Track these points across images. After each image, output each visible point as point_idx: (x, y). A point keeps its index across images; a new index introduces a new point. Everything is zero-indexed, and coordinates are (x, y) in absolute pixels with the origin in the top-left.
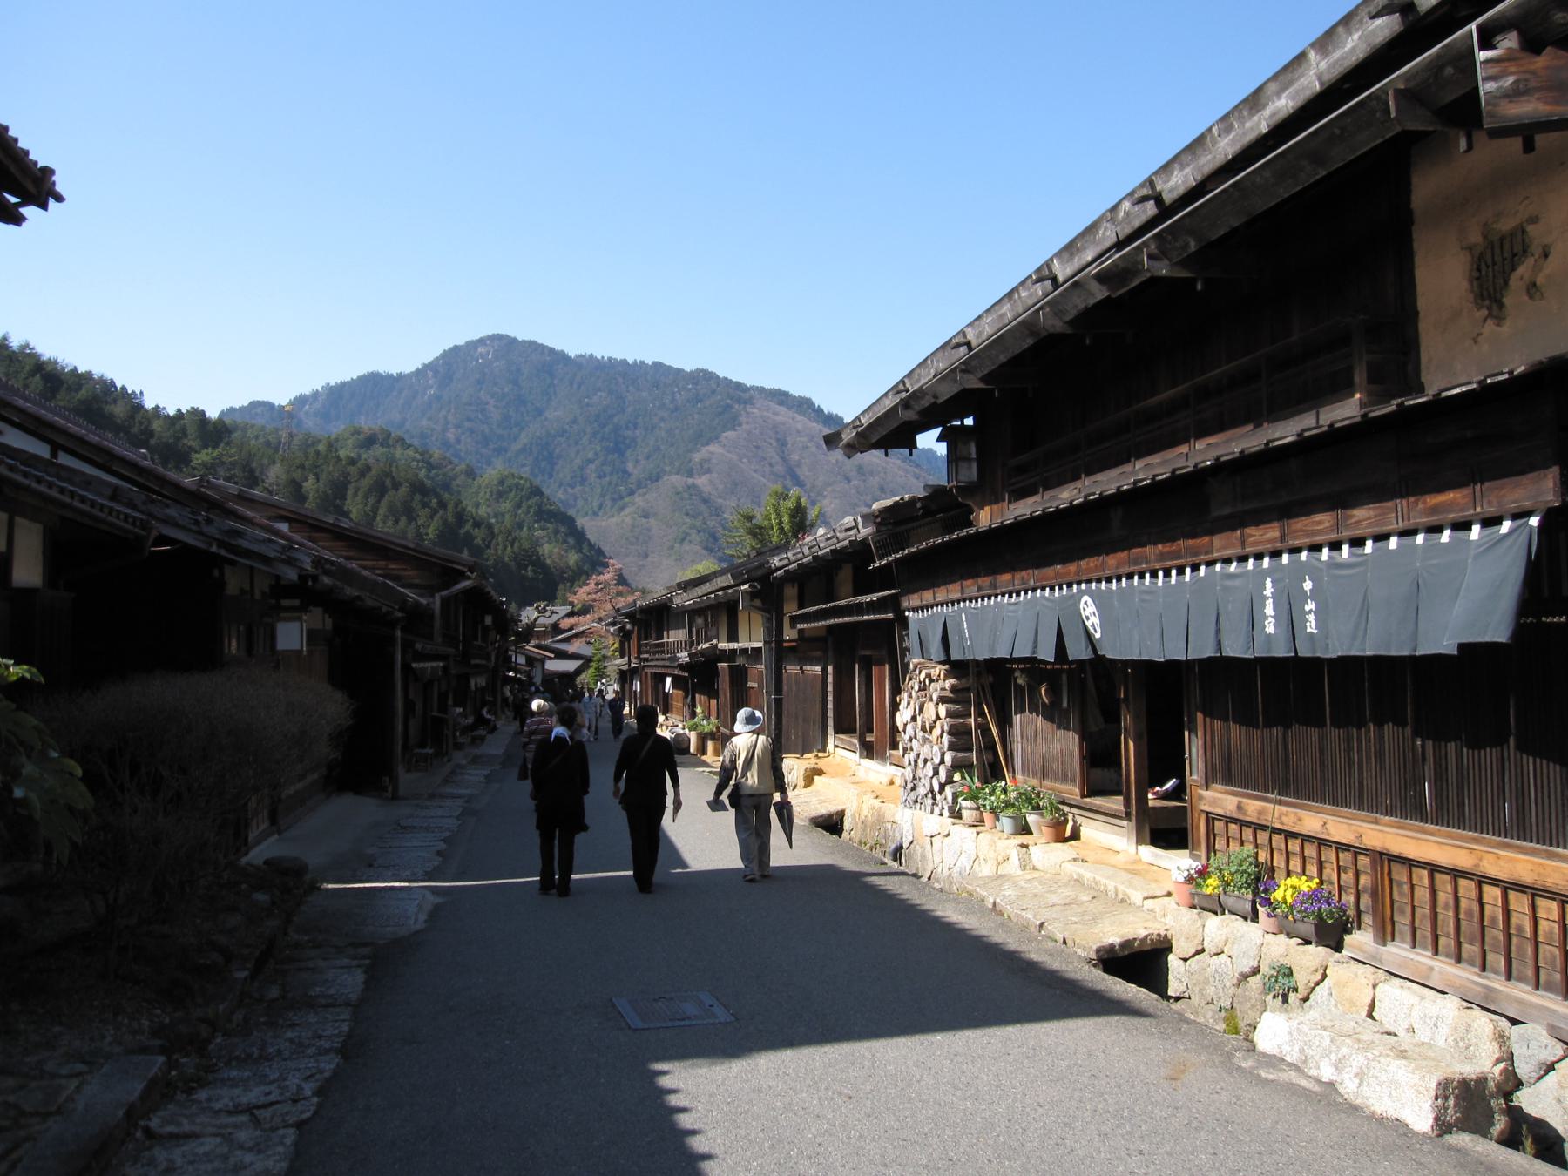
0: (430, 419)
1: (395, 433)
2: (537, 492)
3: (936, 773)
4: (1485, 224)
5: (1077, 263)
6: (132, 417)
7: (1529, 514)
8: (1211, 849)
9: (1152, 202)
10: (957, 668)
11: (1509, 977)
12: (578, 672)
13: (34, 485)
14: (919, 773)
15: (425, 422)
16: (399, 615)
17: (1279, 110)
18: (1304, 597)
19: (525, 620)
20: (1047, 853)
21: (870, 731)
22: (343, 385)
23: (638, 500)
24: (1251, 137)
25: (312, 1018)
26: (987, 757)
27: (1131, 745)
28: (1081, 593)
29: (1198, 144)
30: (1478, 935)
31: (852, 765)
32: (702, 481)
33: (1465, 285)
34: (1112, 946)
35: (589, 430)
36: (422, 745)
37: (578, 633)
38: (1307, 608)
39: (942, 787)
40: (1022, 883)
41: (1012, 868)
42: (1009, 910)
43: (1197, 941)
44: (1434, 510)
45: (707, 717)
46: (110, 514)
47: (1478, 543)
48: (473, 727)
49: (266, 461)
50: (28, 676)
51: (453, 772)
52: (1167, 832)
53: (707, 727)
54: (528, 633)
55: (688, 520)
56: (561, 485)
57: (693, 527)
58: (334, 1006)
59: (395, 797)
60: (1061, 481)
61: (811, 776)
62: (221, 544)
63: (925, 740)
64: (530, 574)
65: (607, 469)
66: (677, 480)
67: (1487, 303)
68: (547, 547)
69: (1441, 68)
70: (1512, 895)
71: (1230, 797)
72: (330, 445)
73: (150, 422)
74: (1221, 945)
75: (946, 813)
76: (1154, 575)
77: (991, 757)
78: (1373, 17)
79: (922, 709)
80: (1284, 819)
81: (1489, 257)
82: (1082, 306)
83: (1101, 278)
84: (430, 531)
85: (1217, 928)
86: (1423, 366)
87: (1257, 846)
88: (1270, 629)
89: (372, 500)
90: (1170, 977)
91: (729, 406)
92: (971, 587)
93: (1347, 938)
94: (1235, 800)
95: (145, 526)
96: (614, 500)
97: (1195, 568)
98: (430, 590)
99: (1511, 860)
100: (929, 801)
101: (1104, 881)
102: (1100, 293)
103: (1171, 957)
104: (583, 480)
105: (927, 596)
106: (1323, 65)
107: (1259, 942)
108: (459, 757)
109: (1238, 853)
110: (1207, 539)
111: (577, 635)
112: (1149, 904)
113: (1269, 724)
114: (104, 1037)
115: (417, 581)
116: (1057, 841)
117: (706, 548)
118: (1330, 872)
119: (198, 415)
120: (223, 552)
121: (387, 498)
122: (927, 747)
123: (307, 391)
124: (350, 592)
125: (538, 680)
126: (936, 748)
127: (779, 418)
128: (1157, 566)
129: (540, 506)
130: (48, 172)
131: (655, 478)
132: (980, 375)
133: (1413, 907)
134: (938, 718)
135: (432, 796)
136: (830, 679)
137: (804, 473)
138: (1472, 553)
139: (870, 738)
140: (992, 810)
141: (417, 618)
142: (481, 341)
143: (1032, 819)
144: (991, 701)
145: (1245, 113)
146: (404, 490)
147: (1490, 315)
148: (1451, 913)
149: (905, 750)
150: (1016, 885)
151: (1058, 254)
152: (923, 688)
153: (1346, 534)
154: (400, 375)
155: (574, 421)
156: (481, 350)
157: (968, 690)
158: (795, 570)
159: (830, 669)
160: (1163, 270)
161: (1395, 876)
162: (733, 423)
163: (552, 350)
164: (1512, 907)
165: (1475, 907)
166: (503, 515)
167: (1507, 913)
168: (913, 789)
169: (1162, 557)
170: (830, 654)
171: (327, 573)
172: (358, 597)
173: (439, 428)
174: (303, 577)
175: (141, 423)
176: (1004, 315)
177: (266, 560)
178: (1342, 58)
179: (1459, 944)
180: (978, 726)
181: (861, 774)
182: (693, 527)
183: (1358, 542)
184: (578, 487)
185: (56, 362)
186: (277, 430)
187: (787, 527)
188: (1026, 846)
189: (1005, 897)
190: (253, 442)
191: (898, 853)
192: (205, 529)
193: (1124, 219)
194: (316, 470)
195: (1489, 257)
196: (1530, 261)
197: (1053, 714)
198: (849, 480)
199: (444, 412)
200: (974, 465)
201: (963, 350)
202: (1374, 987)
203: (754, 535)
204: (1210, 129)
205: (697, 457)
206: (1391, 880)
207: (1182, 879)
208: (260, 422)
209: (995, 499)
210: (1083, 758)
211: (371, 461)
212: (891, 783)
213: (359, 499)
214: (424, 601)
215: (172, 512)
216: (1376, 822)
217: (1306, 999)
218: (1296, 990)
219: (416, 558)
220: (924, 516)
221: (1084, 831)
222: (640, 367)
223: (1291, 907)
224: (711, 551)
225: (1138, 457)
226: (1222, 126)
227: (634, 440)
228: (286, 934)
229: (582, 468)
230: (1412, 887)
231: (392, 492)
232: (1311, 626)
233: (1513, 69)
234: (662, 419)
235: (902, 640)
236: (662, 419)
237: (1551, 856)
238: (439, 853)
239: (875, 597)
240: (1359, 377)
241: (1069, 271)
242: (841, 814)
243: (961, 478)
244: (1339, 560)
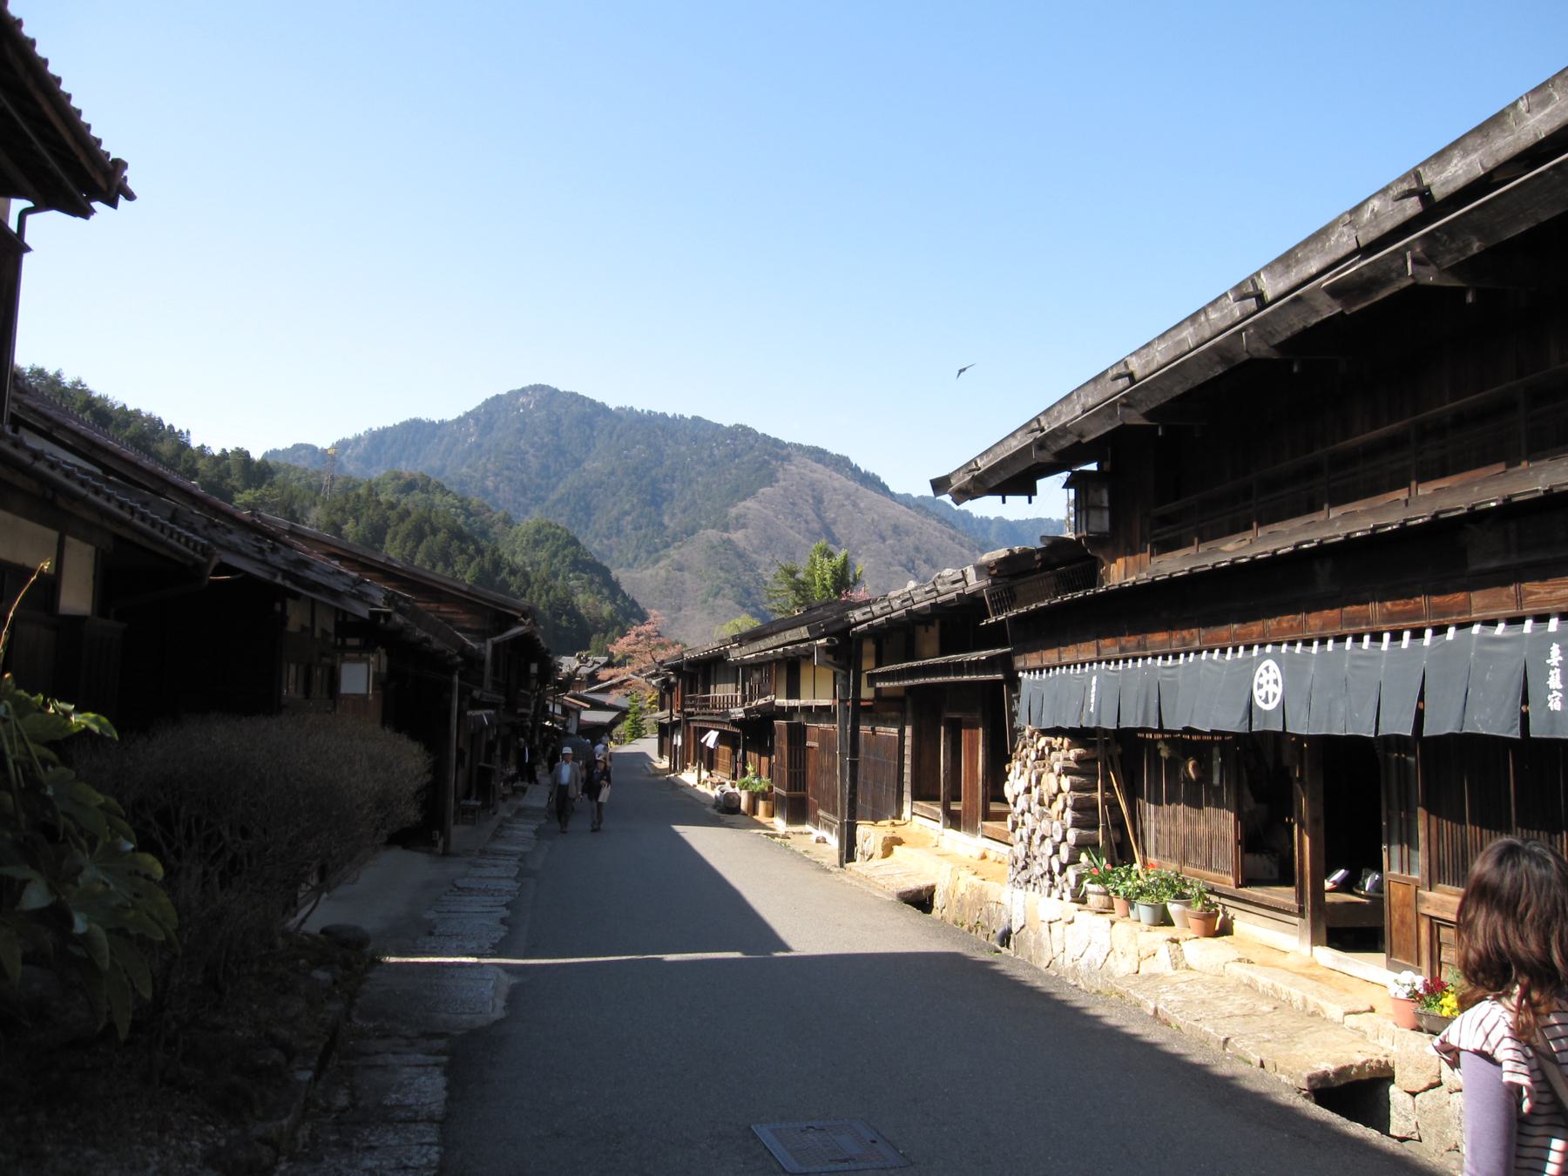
1: (434, 479)
2: (574, 542)
3: (1056, 851)
5: (1294, 277)
6: (178, 456)
9: (1415, 199)
12: (614, 724)
13: (92, 496)
14: (1035, 850)
15: (464, 470)
16: (459, 659)
19: (565, 670)
20: (1205, 953)
22: (385, 430)
25: (392, 1139)
32: (737, 536)
34: (1326, 1074)
37: (617, 685)
39: (1063, 868)
40: (1183, 986)
41: (1162, 964)
42: (1178, 1019)
45: (758, 775)
46: (171, 536)
48: (514, 779)
49: (307, 503)
50: (95, 728)
51: (501, 826)
52: (1354, 932)
54: (570, 681)
55: (722, 574)
56: (597, 536)
57: (727, 581)
58: (415, 1121)
60: (1238, 526)
61: (890, 845)
62: (287, 575)
63: (1043, 815)
64: (564, 624)
65: (643, 521)
66: (712, 534)
68: (581, 596)
72: (370, 489)
73: (195, 461)
75: (1067, 896)
77: (1118, 836)
79: (1040, 783)
83: (1334, 291)
84: (467, 577)
89: (410, 545)
90: (1392, 1113)
91: (768, 462)
95: (206, 552)
96: (649, 552)
98: (482, 635)
100: (1046, 882)
101: (1286, 989)
102: (1329, 309)
103: (1392, 1089)
104: (619, 532)
105: (1050, 656)
110: (1461, 596)
114: (147, 1165)
115: (468, 625)
116: (1208, 935)
117: (739, 603)
119: (243, 456)
120: (288, 584)
121: (425, 543)
122: (1045, 823)
123: (350, 436)
125: (573, 730)
126: (1057, 824)
130: (120, 165)
132: (1144, 409)
134: (1060, 790)
135: (483, 853)
136: (908, 742)
137: (839, 530)
139: (954, 807)
140: (1127, 898)
141: (472, 661)
142: (523, 391)
143: (1174, 909)
144: (1118, 769)
146: (442, 536)
149: (1015, 824)
150: (1174, 986)
151: (1269, 268)
152: (1041, 757)
154: (442, 423)
155: (612, 473)
156: (522, 400)
159: (908, 731)
160: (1430, 278)
162: (770, 479)
163: (592, 402)
166: (539, 564)
168: (1024, 868)
169: (1390, 617)
171: (400, 610)
172: (426, 640)
173: (478, 476)
174: (375, 615)
175: (186, 461)
176: (1184, 340)
177: (334, 594)
180: (1105, 801)
182: (727, 581)
184: (614, 539)
185: (106, 399)
186: (319, 473)
187: (828, 583)
188: (1177, 941)
189: (1167, 1001)
190: (295, 484)
191: (1005, 938)
192: (271, 558)
193: (1370, 221)
194: (356, 514)
198: (884, 539)
200: (1106, 515)
203: (798, 591)
204: (1514, 105)
207: (1404, 996)
208: (302, 464)
209: (1132, 550)
210: (1238, 842)
211: (410, 506)
212: (984, 857)
213: (397, 543)
214: (475, 646)
215: (235, 538)
220: (1043, 569)
221: (1238, 926)
222: (679, 421)
226: (1534, 99)
227: (671, 494)
228: (349, 1019)
229: (618, 520)
231: (430, 538)
234: (700, 474)
235: (1011, 704)
236: (700, 474)
238: (503, 921)
241: (1282, 286)
242: (931, 890)
243: (1092, 528)
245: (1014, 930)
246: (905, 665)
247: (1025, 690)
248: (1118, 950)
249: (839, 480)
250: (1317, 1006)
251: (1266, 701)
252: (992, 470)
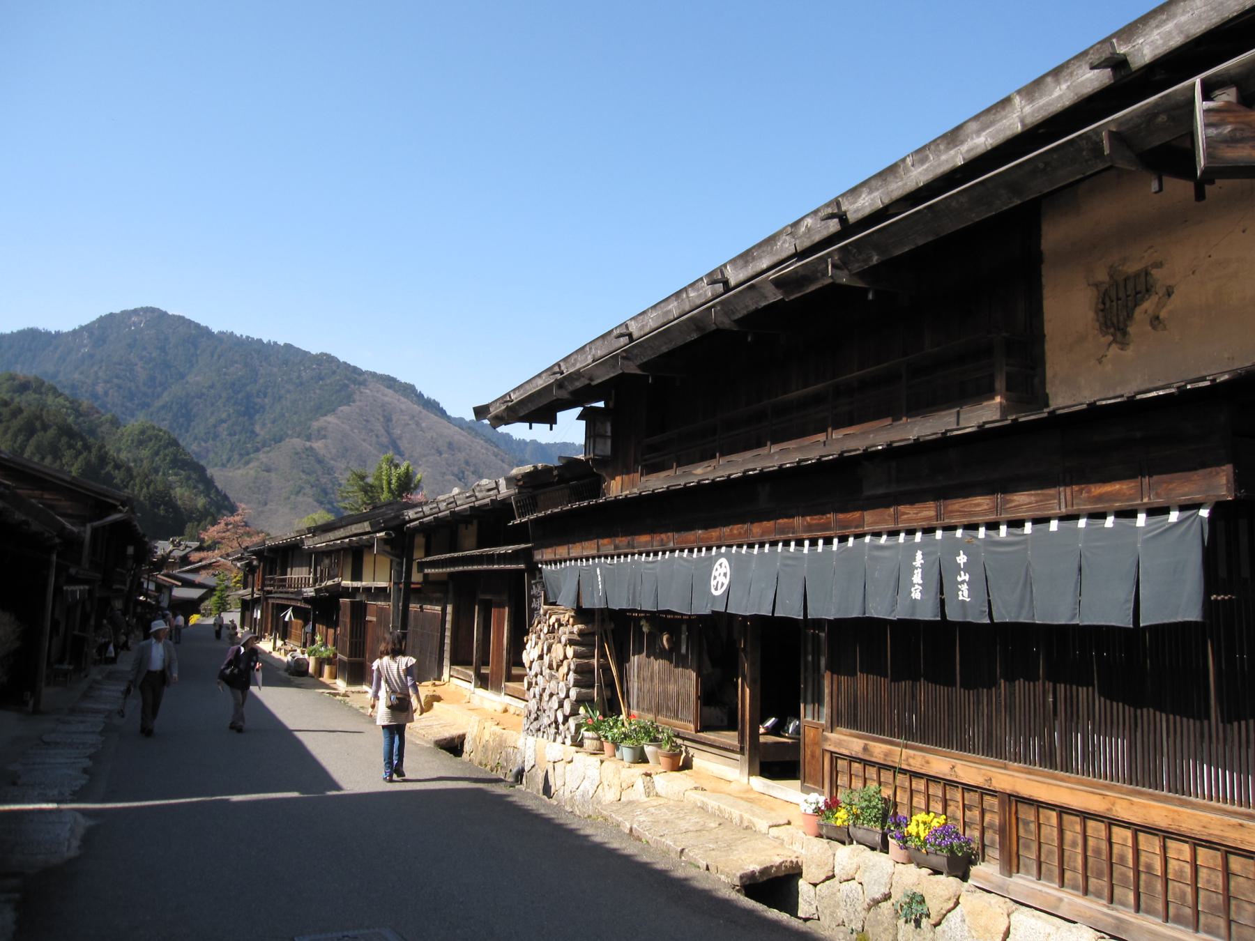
0: (81, 373)
1: (48, 382)
2: (174, 443)
3: (561, 706)
4: (1111, 267)
5: (751, 270)
7: (1198, 506)
8: (834, 786)
9: (836, 220)
10: (582, 614)
11: (1137, 909)
12: (202, 599)
15: (76, 376)
16: (57, 540)
17: (977, 147)
18: (957, 569)
19: (160, 552)
20: (670, 783)
21: (486, 663)
23: (262, 456)
24: (945, 168)
26: (606, 693)
27: (748, 690)
28: (719, 555)
29: (892, 170)
30: (1106, 871)
32: (318, 445)
33: (1091, 314)
34: (753, 873)
35: (224, 395)
36: (61, 661)
37: (207, 570)
38: (959, 579)
39: (566, 719)
40: (653, 810)
41: (638, 793)
42: (647, 836)
43: (829, 867)
44: (1099, 499)
45: (325, 644)
47: (1145, 530)
52: (778, 764)
53: (326, 652)
54: (164, 562)
55: (304, 476)
56: (195, 438)
59: (36, 711)
63: (552, 677)
64: (162, 512)
65: (238, 428)
66: (297, 443)
67: (1112, 330)
68: (178, 490)
69: (1156, 115)
70: (1141, 836)
71: (855, 740)
74: (851, 873)
75: (568, 741)
76: (800, 543)
77: (609, 693)
78: (1092, 68)
79: (550, 651)
80: (911, 761)
81: (1113, 294)
82: (752, 307)
83: (779, 283)
85: (847, 857)
86: (1048, 380)
87: (880, 784)
88: (916, 594)
89: (21, 438)
90: (800, 900)
91: (347, 386)
92: (607, 545)
93: (974, 870)
94: (861, 743)
96: (241, 455)
97: (843, 539)
98: (83, 521)
99: (1145, 806)
100: (553, 730)
101: (729, 809)
102: (774, 296)
103: (801, 882)
104: (216, 437)
105: (562, 551)
106: (1028, 109)
107: (890, 871)
108: (95, 673)
109: (860, 791)
110: (857, 514)
111: (204, 567)
112: (774, 831)
113: (895, 679)
115: (70, 511)
117: (318, 501)
118: (956, 810)
124: (19, 516)
125: (165, 604)
126: (562, 684)
127: (386, 399)
128: (805, 535)
129: (175, 455)
131: (278, 439)
132: (639, 362)
133: (1040, 843)
134: (566, 657)
136: (449, 618)
137: (404, 444)
138: (1140, 539)
141: (71, 544)
142: (135, 311)
143: (649, 750)
144: (611, 641)
145: (942, 147)
146: (52, 432)
147: (1114, 341)
148: (1079, 850)
149: (530, 685)
152: (552, 630)
153: (1006, 516)
154: (58, 334)
155: (212, 387)
156: (134, 319)
157: (593, 634)
158: (430, 522)
159: (449, 609)
161: (1021, 816)
162: (349, 400)
163: (197, 325)
164: (1141, 847)
165: (1104, 846)
167: (1137, 852)
168: (536, 719)
169: (809, 528)
170: (451, 595)
172: (26, 522)
176: (670, 311)
178: (1048, 104)
179: (1086, 878)
180: (600, 666)
181: (476, 701)
183: (1016, 524)
184: (211, 442)
189: (638, 821)
193: (805, 233)
195: (1113, 294)
196: (1155, 298)
197: (672, 656)
198: (440, 454)
199: (95, 368)
200: (609, 442)
201: (624, 340)
202: (1009, 916)
203: (366, 492)
204: (904, 160)
205: (316, 425)
206: (1017, 819)
210: (698, 698)
211: (23, 405)
212: (506, 711)
213: (9, 436)
216: (1005, 768)
217: (938, 924)
218: (928, 916)
219: (70, 490)
220: (559, 483)
221: (696, 762)
222: (273, 346)
223: (925, 842)
224: (321, 503)
225: (774, 442)
229: (215, 426)
230: (1039, 825)
231: (41, 434)
232: (964, 594)
233: (1231, 119)
234: (288, 391)
236: (288, 391)
237: (1184, 804)
238: (85, 771)
239: (509, 549)
240: (1000, 384)
241: (742, 276)
242: (462, 738)
243: (597, 452)
244: (997, 538)
248: (605, 783)
249: (405, 404)
250: (750, 821)
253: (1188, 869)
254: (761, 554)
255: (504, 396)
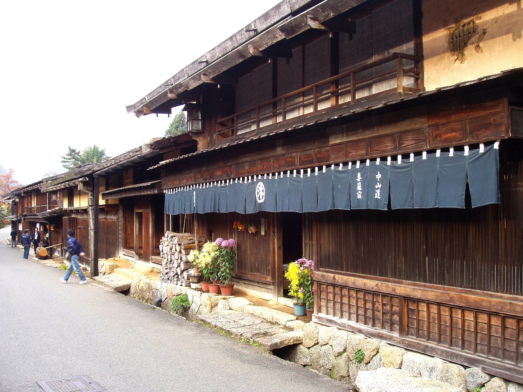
3: (179, 266)
7: (493, 142)
18: (376, 181)
28: (258, 181)
31: (132, 263)
38: (376, 187)
39: (182, 272)
43: (315, 340)
61: (112, 269)
75: (184, 284)
83: (283, 29)
88: (359, 197)
99: (404, 287)
100: (176, 279)
102: (281, 36)
138: (467, 162)
167: (464, 321)
196: (477, 36)
200: (200, 123)
202: (402, 355)
239: (149, 184)
241: (264, 27)
243: (194, 128)
244: (396, 165)
245: (163, 300)
246: (117, 189)
247: (166, 198)
248: (203, 304)
251: (260, 199)
252: (151, 102)
253: (486, 326)
254: (279, 178)
255: (142, 99)
